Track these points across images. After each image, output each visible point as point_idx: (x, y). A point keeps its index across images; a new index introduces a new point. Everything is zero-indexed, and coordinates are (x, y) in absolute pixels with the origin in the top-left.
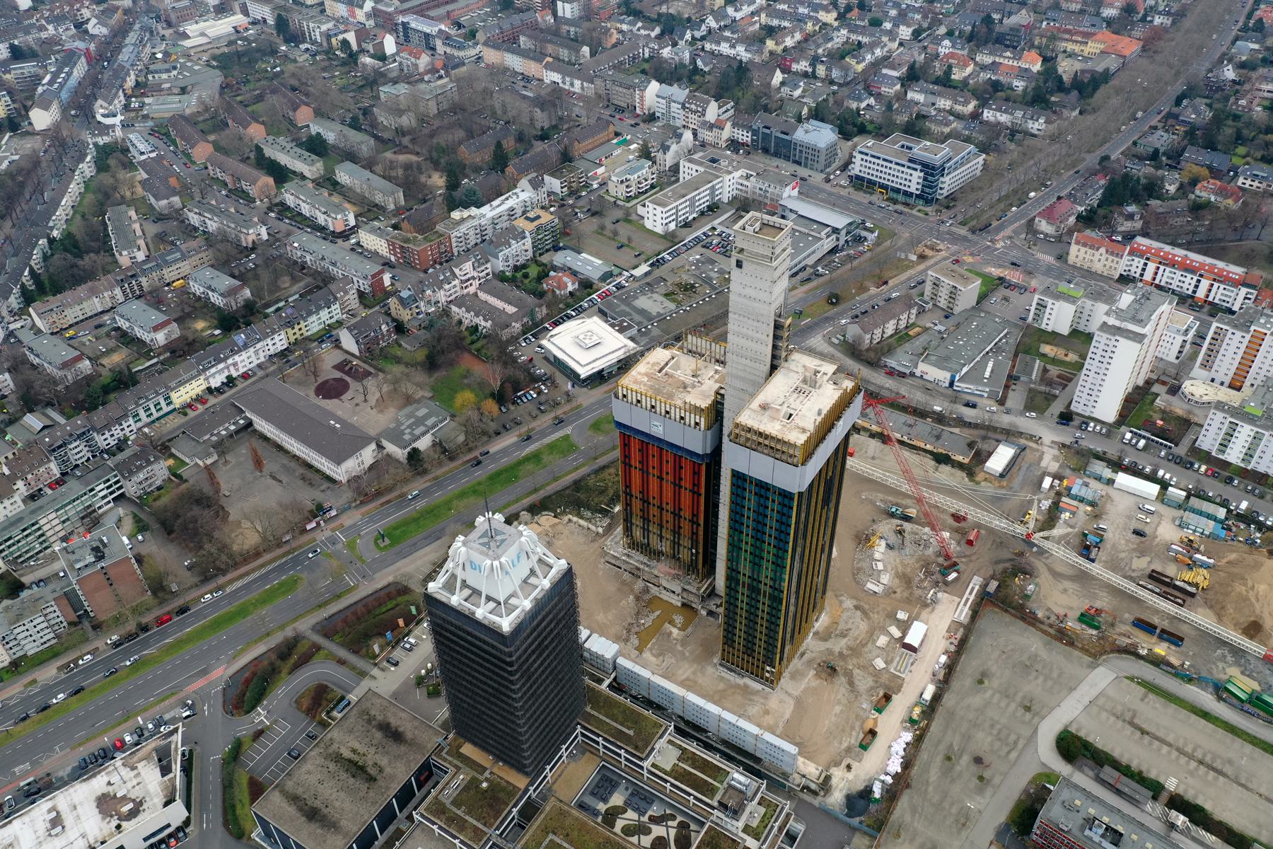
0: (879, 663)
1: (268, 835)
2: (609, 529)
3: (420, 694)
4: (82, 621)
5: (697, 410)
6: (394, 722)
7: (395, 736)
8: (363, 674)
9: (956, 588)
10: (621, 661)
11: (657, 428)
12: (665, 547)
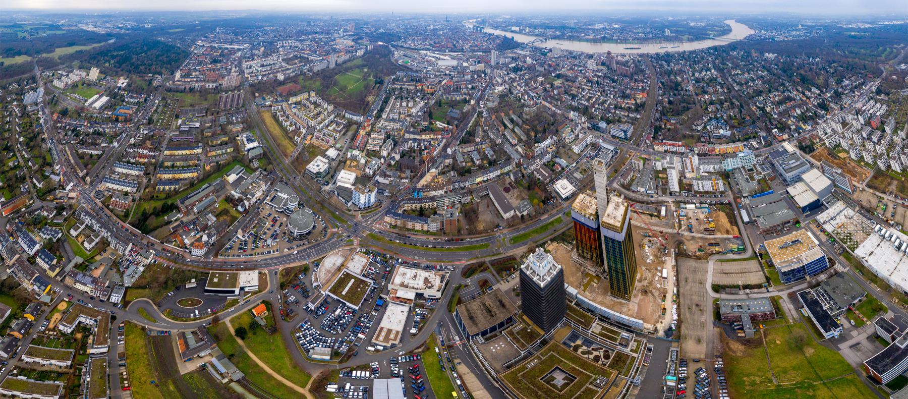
0: (659, 286)
1: (457, 316)
2: (572, 249)
3: (513, 294)
4: (442, 231)
5: (592, 215)
6: (504, 301)
7: (503, 305)
8: (498, 282)
9: (668, 255)
10: (579, 296)
11: (583, 220)
12: (589, 256)
